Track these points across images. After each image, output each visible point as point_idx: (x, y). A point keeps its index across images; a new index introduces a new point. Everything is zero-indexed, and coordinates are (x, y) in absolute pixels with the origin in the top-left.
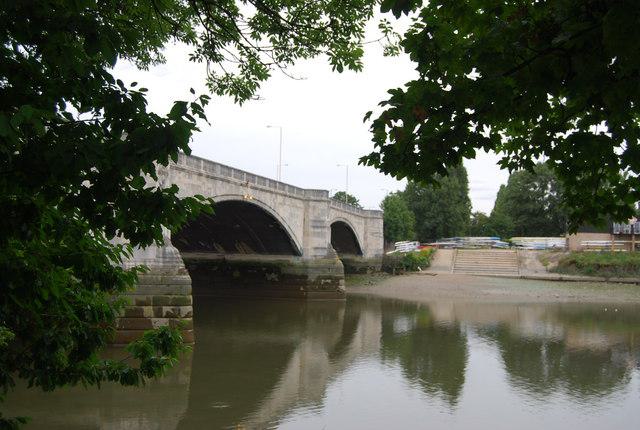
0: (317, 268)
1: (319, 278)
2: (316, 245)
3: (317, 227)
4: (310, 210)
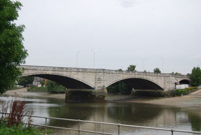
0: (98, 93)
1: (99, 96)
2: (99, 86)
3: (99, 80)
4: (97, 75)
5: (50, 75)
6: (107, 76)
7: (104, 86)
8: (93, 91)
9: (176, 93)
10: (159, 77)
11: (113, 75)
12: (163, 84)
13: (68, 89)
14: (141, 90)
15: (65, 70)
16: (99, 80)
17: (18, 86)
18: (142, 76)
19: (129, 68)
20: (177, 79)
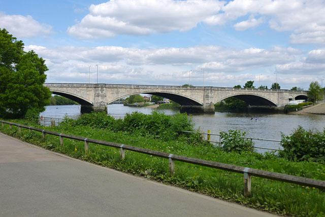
5: (159, 93)
6: (216, 93)
7: (211, 103)
8: (202, 107)
9: (288, 110)
10: (271, 94)
11: (222, 92)
12: (277, 100)
13: (181, 105)
14: (256, 106)
15: (220, 89)
16: (207, 96)
17: (150, 103)
18: (252, 93)
19: (246, 84)
20: (292, 94)
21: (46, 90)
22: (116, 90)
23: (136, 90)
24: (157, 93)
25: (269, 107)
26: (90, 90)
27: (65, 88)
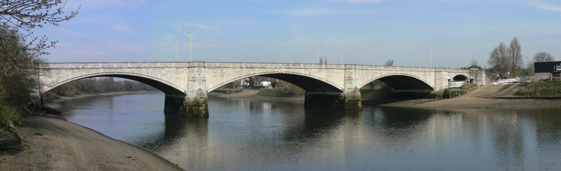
4: (346, 73)
8: (342, 94)
18: (405, 72)
21: (197, 104)
22: (219, 70)
23: (250, 70)
24: (279, 74)
25: (422, 91)
26: (181, 72)
27: (144, 70)
